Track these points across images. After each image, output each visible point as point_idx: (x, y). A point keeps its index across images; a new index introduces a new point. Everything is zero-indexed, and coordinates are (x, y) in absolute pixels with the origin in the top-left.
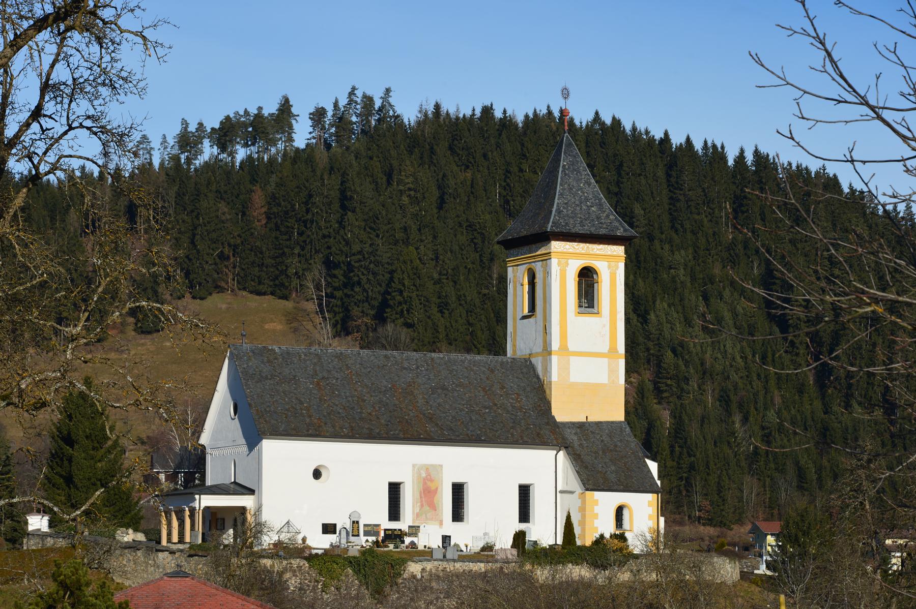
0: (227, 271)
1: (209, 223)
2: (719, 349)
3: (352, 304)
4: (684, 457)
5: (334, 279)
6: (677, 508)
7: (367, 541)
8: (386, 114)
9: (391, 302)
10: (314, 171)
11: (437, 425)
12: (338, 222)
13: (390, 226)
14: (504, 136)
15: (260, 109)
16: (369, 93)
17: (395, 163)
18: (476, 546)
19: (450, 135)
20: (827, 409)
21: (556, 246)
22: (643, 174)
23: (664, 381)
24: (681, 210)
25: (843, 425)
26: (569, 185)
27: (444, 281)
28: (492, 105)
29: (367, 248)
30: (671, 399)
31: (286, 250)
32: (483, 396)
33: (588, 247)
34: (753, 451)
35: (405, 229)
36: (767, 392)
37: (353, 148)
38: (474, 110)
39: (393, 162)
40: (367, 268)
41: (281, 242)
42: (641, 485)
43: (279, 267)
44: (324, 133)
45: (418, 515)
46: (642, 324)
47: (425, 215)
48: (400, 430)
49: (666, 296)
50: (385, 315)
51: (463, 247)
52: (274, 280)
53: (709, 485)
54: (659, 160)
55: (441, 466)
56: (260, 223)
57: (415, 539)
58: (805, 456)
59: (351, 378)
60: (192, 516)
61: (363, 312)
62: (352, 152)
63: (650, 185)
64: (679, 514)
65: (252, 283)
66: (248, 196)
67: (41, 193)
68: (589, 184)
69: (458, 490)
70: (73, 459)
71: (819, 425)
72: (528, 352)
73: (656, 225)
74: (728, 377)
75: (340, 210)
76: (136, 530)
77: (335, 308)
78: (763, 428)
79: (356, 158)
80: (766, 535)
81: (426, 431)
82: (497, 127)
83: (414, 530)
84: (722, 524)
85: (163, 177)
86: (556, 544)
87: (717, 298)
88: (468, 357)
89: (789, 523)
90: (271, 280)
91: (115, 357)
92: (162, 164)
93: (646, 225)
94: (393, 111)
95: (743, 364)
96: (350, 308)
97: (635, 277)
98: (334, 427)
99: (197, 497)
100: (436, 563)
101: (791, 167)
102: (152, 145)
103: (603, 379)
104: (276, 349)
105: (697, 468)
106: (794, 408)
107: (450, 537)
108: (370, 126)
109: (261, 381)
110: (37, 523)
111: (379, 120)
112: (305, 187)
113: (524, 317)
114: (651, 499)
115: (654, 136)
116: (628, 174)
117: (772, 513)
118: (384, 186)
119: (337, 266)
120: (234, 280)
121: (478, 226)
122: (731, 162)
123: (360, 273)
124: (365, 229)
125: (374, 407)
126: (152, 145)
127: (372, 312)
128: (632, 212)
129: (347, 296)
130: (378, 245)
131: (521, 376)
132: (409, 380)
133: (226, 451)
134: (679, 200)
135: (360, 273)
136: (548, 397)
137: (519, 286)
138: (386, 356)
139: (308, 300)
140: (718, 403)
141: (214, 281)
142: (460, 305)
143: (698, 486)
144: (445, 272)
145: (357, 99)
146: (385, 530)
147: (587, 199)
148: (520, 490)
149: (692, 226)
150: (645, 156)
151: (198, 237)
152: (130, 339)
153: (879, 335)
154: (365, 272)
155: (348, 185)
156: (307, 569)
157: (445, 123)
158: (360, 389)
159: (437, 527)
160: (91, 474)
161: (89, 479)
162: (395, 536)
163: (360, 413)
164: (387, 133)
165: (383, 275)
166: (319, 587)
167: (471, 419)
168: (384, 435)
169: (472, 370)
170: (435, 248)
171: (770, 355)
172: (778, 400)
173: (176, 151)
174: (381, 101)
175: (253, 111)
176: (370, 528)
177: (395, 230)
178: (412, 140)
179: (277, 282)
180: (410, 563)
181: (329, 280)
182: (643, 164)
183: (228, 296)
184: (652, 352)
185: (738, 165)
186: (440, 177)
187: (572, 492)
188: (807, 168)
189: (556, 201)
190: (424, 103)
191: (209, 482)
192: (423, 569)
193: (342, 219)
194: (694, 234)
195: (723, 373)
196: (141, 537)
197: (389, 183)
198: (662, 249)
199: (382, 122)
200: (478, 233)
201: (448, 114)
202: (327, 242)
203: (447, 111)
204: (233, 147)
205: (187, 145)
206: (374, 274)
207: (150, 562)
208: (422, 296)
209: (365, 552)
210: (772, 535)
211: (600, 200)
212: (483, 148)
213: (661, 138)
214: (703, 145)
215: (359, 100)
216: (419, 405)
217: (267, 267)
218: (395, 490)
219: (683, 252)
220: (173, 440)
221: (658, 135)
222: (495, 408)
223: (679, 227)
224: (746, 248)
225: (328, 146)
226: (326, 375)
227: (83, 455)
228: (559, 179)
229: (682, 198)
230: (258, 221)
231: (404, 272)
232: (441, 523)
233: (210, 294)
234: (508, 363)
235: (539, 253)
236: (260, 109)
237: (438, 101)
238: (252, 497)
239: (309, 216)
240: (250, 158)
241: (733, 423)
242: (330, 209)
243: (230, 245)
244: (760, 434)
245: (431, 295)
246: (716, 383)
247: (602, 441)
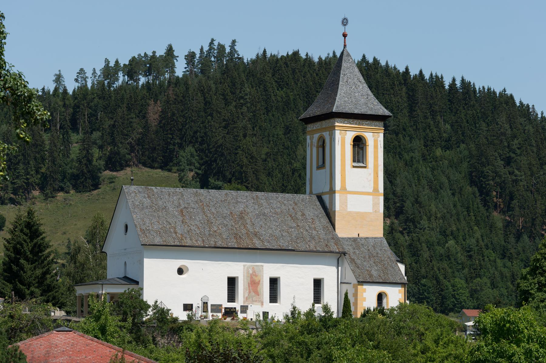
15: (154, 52)
16: (222, 43)
45: (247, 298)
83: (244, 309)
92: (92, 87)
102: (87, 75)
107: (268, 313)
122: (447, 87)
126: (87, 75)
132: (241, 209)
145: (215, 47)
159: (260, 306)
174: (230, 48)
175: (150, 54)
204: (137, 77)
215: (216, 47)
226: (186, 206)
232: (262, 304)
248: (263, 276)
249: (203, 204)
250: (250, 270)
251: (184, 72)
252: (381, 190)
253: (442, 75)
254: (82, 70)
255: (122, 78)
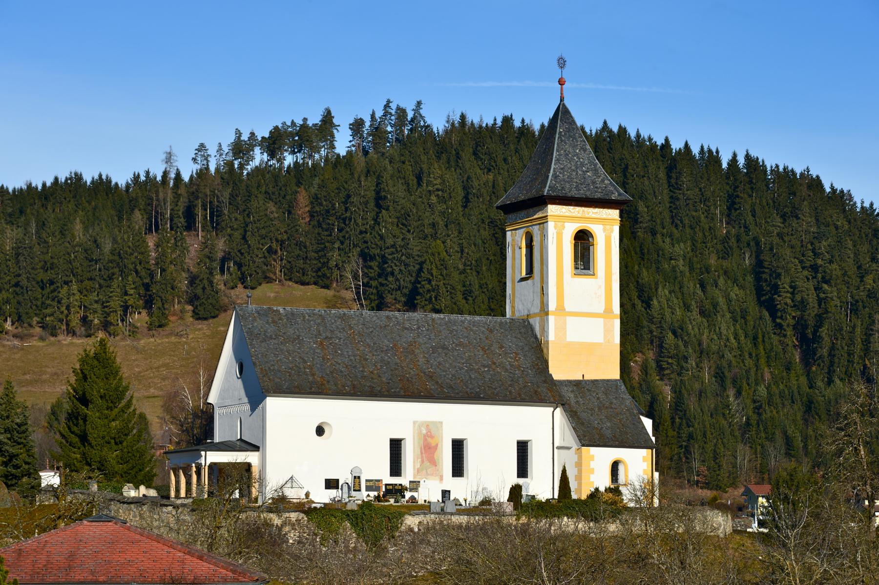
0: (275, 263)
1: (258, 220)
2: (715, 331)
3: (387, 292)
4: (683, 427)
5: (371, 271)
6: (678, 473)
7: (368, 496)
8: (417, 124)
9: (421, 291)
10: (352, 174)
11: (437, 383)
12: (373, 219)
13: (420, 222)
14: (522, 142)
15: (305, 120)
16: (402, 106)
17: (425, 166)
18: (475, 501)
19: (474, 142)
20: (812, 384)
21: (553, 210)
22: (646, 175)
23: (666, 359)
24: (680, 208)
25: (827, 398)
26: (565, 151)
27: (468, 271)
28: (512, 116)
29: (399, 242)
30: (672, 376)
31: (327, 244)
32: (483, 355)
33: (583, 211)
34: (745, 421)
35: (433, 225)
36: (757, 366)
37: (387, 154)
38: (495, 120)
39: (423, 166)
40: (399, 260)
41: (323, 237)
42: (637, 441)
43: (321, 260)
44: (363, 142)
45: (418, 471)
46: (646, 309)
47: (451, 212)
48: (401, 388)
49: (668, 284)
50: (416, 302)
51: (486, 241)
52: (317, 272)
53: (706, 453)
54: (660, 163)
55: (441, 423)
56: (304, 221)
57: (415, 494)
58: (792, 427)
59: (354, 338)
60: (198, 473)
61: (395, 299)
62: (387, 157)
63: (652, 185)
64: (680, 478)
65: (297, 274)
66: (293, 196)
67: (110, 195)
68: (585, 150)
69: (458, 446)
70: (88, 418)
71: (805, 399)
72: (526, 313)
73: (658, 221)
74: (723, 356)
75: (375, 209)
76: (148, 487)
77: (371, 296)
78: (754, 401)
79: (391, 162)
80: (758, 497)
81: (426, 389)
82: (516, 135)
83: (415, 485)
84: (718, 488)
85: (218, 181)
86: (553, 498)
87: (712, 286)
88: (468, 318)
89: (779, 482)
90: (314, 272)
91: (175, 341)
92: (217, 170)
93: (649, 221)
94: (424, 121)
95: (736, 344)
96: (385, 296)
97: (639, 267)
98: (336, 385)
99: (203, 453)
100: (432, 516)
101: (778, 169)
102: (209, 152)
103: (599, 338)
104: (281, 310)
105: (695, 437)
106: (782, 383)
107: (449, 491)
108: (403, 135)
109: (265, 341)
110: (50, 478)
111: (411, 130)
112: (344, 188)
113: (523, 280)
114: (645, 455)
115: (656, 142)
116: (633, 176)
117: (763, 478)
118: (415, 187)
119: (372, 258)
120: (281, 271)
121: (499, 222)
122: (725, 165)
123: (393, 265)
124: (398, 226)
125: (376, 366)
127: (403, 299)
128: (636, 209)
129: (382, 285)
130: (409, 239)
131: (519, 336)
132: (410, 339)
133: (231, 410)
134: (678, 199)
135: (393, 265)
136: (545, 356)
137: (517, 249)
138: (388, 317)
139: (347, 289)
140: (713, 379)
141: (264, 272)
142: (483, 292)
143: (696, 453)
144: (469, 263)
145: (391, 111)
146: (386, 485)
147: (582, 165)
148: (518, 446)
149: (691, 221)
150: (648, 160)
151: (249, 233)
152: (189, 324)
153: (858, 318)
154: (398, 264)
155: (382, 186)
156: (305, 523)
157: (469, 131)
158: (362, 348)
159: (438, 482)
160: (105, 433)
161: (103, 438)
162: (396, 491)
163: (362, 371)
164: (418, 141)
165: (414, 267)
166: (318, 540)
167: (470, 377)
168: (386, 393)
169: (472, 330)
170: (461, 242)
171: (760, 336)
172: (767, 376)
173: (230, 158)
174: (413, 112)
175: (299, 122)
176: (371, 484)
177: (424, 226)
178: (440, 147)
179: (320, 273)
180: (407, 516)
181: (366, 271)
182: (646, 166)
183: (275, 286)
184: (655, 333)
185: (731, 168)
186: (465, 179)
187: (568, 448)
188: (792, 171)
189: (553, 166)
190: (451, 114)
191: (217, 439)
192: (420, 522)
193: (377, 217)
194: (692, 229)
195: (718, 353)
196: (152, 493)
197: (419, 184)
198: (664, 242)
199: (414, 132)
200: (499, 228)
201: (472, 123)
202: (364, 237)
203: (472, 122)
205: (240, 152)
206: (406, 265)
207: (155, 516)
208: (448, 284)
209: (366, 505)
210: (763, 497)
211: (595, 165)
212: (503, 153)
213: (662, 144)
214: (699, 150)
215: (393, 112)
216: (420, 364)
217: (310, 260)
218: (396, 446)
219: (682, 245)
220: (186, 400)
221: (660, 141)
222: (494, 367)
223: (679, 222)
224: (738, 241)
225: (366, 153)
226: (329, 335)
227: (97, 414)
228: (556, 146)
229: (681, 196)
230: (302, 219)
231: (432, 263)
233: (260, 284)
234: (506, 323)
235: (535, 217)
236: (305, 120)
237: (464, 112)
238: (256, 453)
239: (348, 214)
240: (296, 163)
241: (728, 396)
242: (367, 208)
243: (277, 240)
244: (752, 407)
245: (456, 284)
246: (712, 362)
247: (598, 398)
248: (442, 437)
249: (354, 332)
250: (422, 428)
251: (348, 147)
252: (616, 309)
253: (717, 149)
254: (202, 145)
255: (259, 157)
